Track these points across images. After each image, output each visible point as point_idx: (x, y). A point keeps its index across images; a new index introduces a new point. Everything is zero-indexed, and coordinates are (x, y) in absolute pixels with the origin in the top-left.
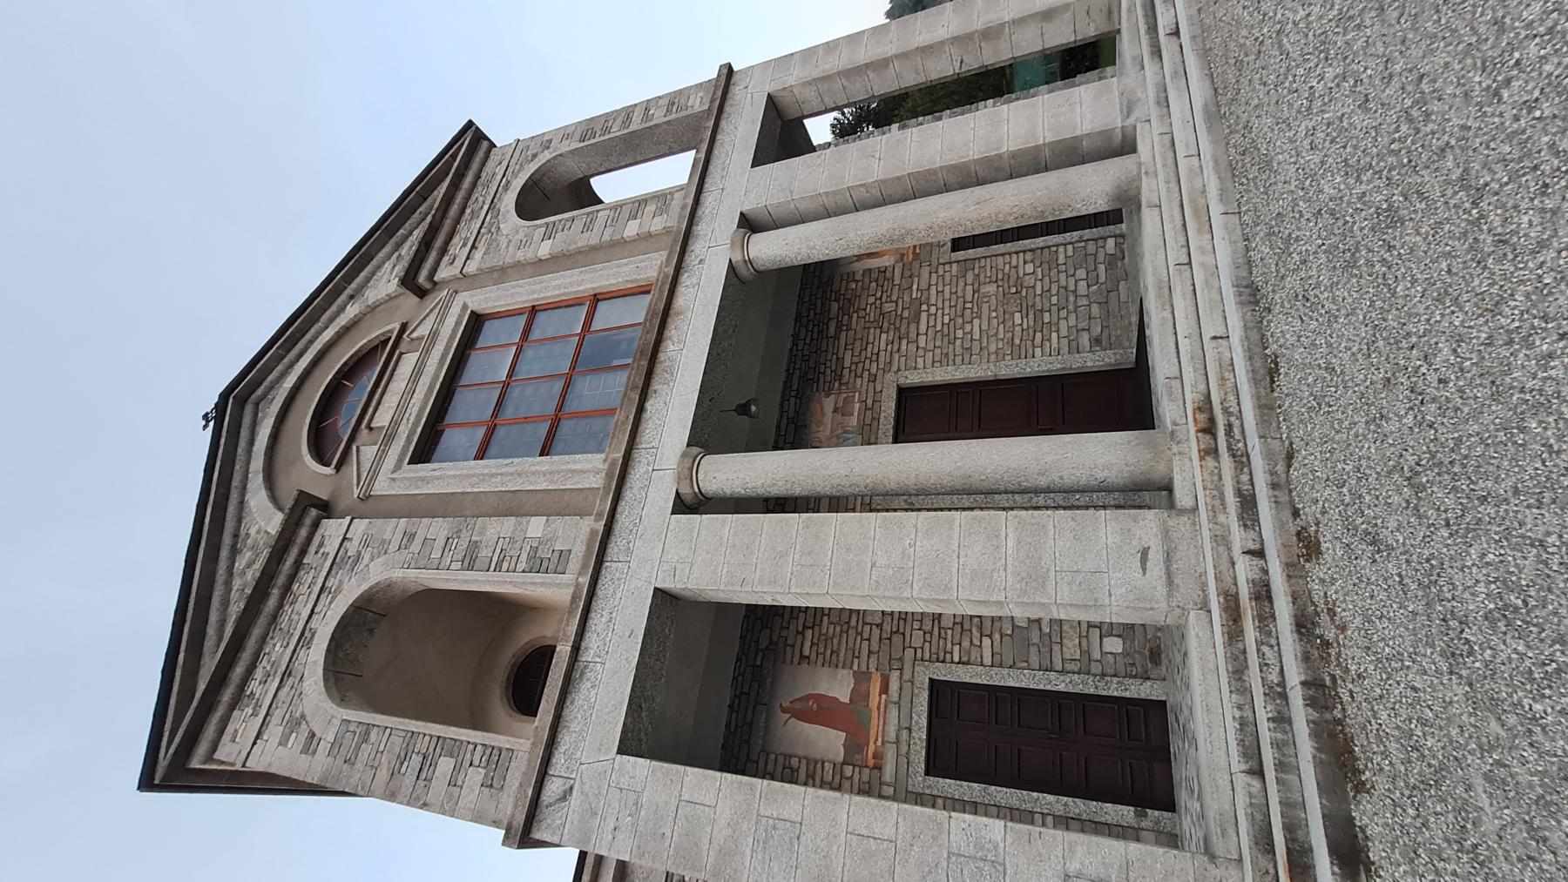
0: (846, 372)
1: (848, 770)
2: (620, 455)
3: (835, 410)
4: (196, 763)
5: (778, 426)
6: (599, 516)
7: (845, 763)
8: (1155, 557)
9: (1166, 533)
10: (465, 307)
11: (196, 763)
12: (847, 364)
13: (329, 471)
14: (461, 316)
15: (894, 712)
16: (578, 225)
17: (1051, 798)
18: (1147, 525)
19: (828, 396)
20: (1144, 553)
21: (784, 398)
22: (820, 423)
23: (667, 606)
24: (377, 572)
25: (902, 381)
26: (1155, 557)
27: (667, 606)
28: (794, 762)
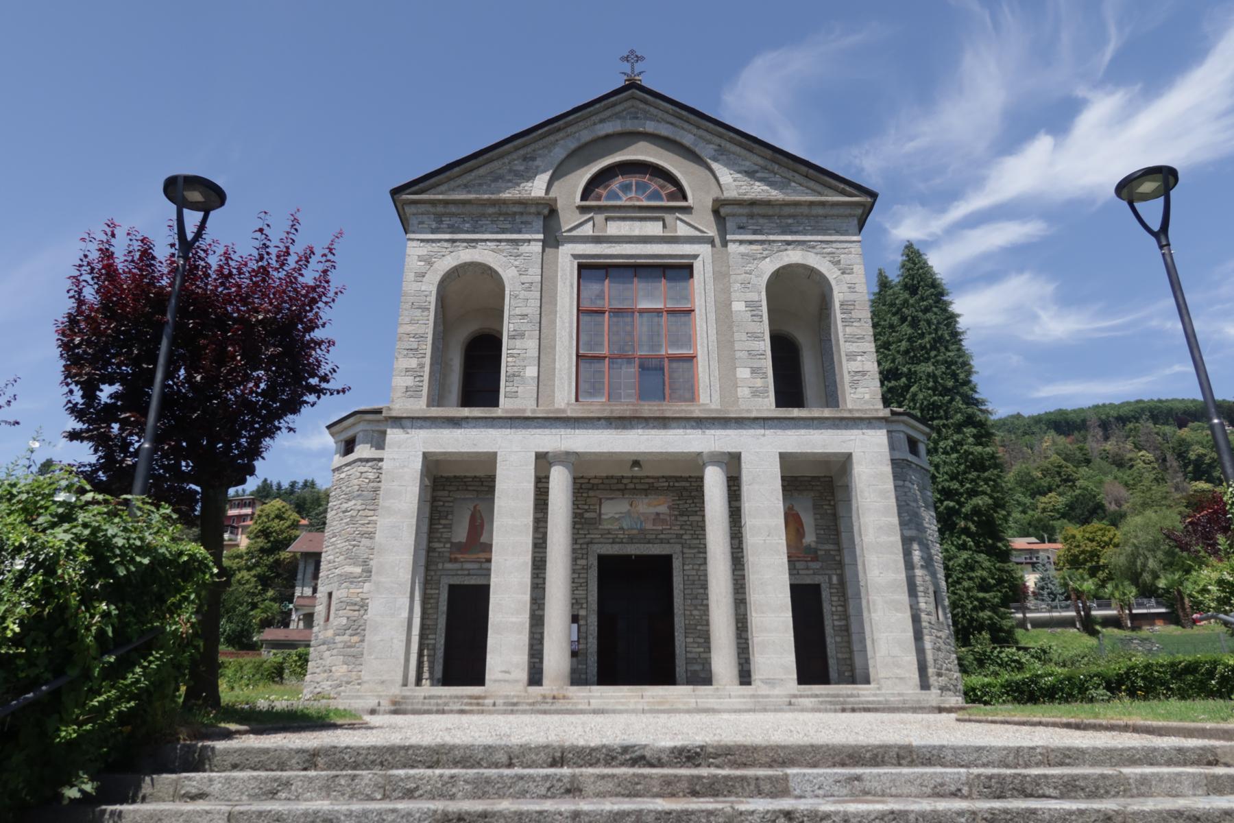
0: (685, 518)
1: (448, 545)
2: (569, 414)
3: (658, 514)
4: (407, 209)
5: (648, 477)
6: (533, 411)
7: (452, 544)
8: (507, 676)
9: (517, 681)
10: (696, 257)
11: (407, 209)
12: (691, 518)
13: (578, 201)
14: (682, 257)
15: (476, 566)
16: (754, 327)
17: (443, 642)
18: (524, 676)
19: (669, 507)
20: (508, 672)
21: (667, 478)
22: (649, 505)
23: (490, 459)
24: (508, 275)
25: (674, 556)
26: (507, 676)
27: (490, 459)
28: (450, 517)
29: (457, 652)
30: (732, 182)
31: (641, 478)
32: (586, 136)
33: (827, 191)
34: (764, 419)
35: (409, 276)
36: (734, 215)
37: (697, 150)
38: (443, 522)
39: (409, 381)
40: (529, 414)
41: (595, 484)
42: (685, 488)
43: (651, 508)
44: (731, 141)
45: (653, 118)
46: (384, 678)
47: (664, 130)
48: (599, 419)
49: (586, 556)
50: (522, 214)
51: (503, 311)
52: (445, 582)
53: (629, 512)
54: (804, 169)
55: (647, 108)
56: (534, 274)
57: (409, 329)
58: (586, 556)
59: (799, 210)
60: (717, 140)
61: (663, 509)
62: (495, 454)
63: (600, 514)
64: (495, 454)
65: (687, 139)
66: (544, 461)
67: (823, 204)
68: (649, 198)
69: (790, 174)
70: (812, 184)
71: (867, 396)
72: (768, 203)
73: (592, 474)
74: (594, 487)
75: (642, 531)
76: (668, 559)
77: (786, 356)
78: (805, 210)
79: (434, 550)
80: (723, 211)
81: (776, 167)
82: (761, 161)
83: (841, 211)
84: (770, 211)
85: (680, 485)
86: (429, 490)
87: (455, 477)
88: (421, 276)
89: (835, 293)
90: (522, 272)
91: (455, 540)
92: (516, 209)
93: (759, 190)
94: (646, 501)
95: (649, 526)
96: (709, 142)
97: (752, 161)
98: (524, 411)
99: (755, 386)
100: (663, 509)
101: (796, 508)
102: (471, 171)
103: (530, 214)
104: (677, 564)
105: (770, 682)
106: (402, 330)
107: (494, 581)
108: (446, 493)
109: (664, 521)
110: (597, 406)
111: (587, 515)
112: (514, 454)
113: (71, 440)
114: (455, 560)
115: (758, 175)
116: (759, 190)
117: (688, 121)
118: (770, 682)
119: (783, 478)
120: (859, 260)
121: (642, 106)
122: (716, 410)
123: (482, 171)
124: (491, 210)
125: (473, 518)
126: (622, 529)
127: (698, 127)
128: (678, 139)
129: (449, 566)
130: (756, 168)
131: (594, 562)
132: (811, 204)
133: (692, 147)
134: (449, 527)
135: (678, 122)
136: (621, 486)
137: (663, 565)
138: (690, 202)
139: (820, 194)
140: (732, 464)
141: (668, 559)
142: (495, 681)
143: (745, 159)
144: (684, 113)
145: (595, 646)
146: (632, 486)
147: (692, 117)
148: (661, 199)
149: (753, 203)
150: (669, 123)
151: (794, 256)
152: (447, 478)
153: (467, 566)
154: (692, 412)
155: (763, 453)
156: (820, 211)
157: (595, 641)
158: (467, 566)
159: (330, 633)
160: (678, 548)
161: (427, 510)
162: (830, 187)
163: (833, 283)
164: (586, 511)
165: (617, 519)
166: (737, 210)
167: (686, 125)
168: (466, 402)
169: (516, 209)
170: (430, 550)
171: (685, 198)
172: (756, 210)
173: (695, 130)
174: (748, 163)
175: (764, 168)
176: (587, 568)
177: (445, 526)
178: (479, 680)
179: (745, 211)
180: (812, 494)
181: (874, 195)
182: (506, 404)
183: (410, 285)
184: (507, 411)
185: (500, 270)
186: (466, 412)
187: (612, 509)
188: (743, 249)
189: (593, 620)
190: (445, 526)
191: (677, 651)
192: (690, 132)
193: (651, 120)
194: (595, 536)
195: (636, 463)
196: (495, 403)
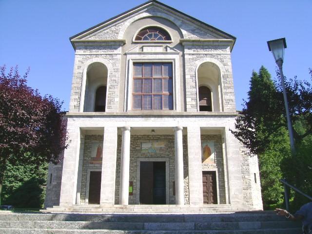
3: (161, 148)
8: (107, 201)
9: (111, 203)
13: (134, 40)
19: (165, 146)
29: (118, 201)
30: (187, 35)
31: (155, 135)
32: (137, 17)
33: (219, 37)
34: (195, 115)
35: (76, 67)
36: (187, 45)
37: (175, 22)
38: (88, 150)
39: (76, 103)
40: (115, 114)
41: (138, 137)
42: (170, 139)
43: (157, 145)
44: (187, 20)
45: (160, 12)
46: (67, 201)
47: (164, 16)
48: (139, 116)
49: (136, 162)
50: (114, 45)
51: (107, 77)
52: (89, 171)
53: (151, 147)
54: (211, 29)
55: (158, 8)
56: (119, 66)
57: (75, 85)
58: (136, 162)
59: (209, 44)
60: (182, 19)
61: (163, 146)
62: (104, 128)
63: (141, 148)
64: (104, 128)
65: (172, 19)
66: (121, 132)
67: (218, 41)
68: (158, 39)
69: (206, 31)
70: (214, 34)
71: (231, 108)
72: (199, 41)
73: (138, 134)
74: (139, 139)
75: (156, 154)
76: (164, 163)
77: (205, 92)
78: (212, 43)
79: (85, 160)
80: (183, 44)
81: (202, 28)
82: (197, 27)
83: (224, 44)
84: (199, 44)
85: (168, 137)
86: (83, 140)
87: (92, 135)
88: (79, 67)
89: (221, 71)
90: (114, 64)
91: (92, 157)
92: (112, 44)
93: (194, 37)
94: (157, 143)
95: (158, 152)
96: (179, 20)
97: (194, 26)
98: (114, 113)
99: (193, 102)
100: (163, 146)
101: (208, 146)
102: (169, 12)
103: (117, 45)
104: (167, 164)
105: (195, 203)
106: (73, 86)
107: (103, 170)
108: (89, 141)
109: (163, 150)
110: (139, 112)
111: (137, 148)
112: (109, 127)
113: (177, 127)
114: (92, 163)
115: (196, 31)
116: (194, 37)
117: (171, 13)
118: (195, 203)
119: (201, 135)
120: (230, 61)
121: (156, 7)
122: (179, 113)
123: (105, 32)
124: (103, 44)
125: (98, 149)
126: (149, 153)
127: (175, 15)
128: (168, 19)
129: (90, 165)
130: (195, 29)
131: (139, 164)
132: (213, 41)
133: (173, 22)
134: (90, 152)
135: (169, 13)
136: (149, 138)
137: (163, 164)
138: (172, 41)
139: (218, 38)
140: (185, 130)
141: (164, 163)
142: (103, 203)
143: (191, 26)
144: (170, 10)
145: (139, 193)
146: (152, 138)
147: (173, 11)
148: (163, 40)
149: (193, 41)
150: (166, 13)
151: (208, 59)
152: (90, 135)
153: (96, 165)
154: (171, 113)
155: (195, 126)
156: (217, 44)
157: (139, 191)
158: (96, 165)
159: (51, 187)
160: (168, 159)
161: (83, 146)
162: (220, 36)
163: (221, 69)
164: (137, 147)
165: (147, 150)
166: (188, 43)
167: (171, 14)
168: (200, 106)
169: (112, 44)
170: (84, 160)
171: (170, 39)
172: (195, 43)
173: (174, 16)
174: (192, 27)
175: (198, 29)
176: (136, 166)
177: (89, 152)
178: (99, 203)
179: (191, 44)
180: (214, 141)
181: (235, 38)
182: (107, 110)
183: (76, 71)
184: (107, 113)
185: (106, 65)
186: (94, 113)
187: (146, 146)
188: (191, 57)
189: (138, 184)
190: (89, 152)
191: (167, 193)
192: (172, 16)
193: (159, 12)
194: (139, 155)
195: (153, 131)
196: (104, 110)
